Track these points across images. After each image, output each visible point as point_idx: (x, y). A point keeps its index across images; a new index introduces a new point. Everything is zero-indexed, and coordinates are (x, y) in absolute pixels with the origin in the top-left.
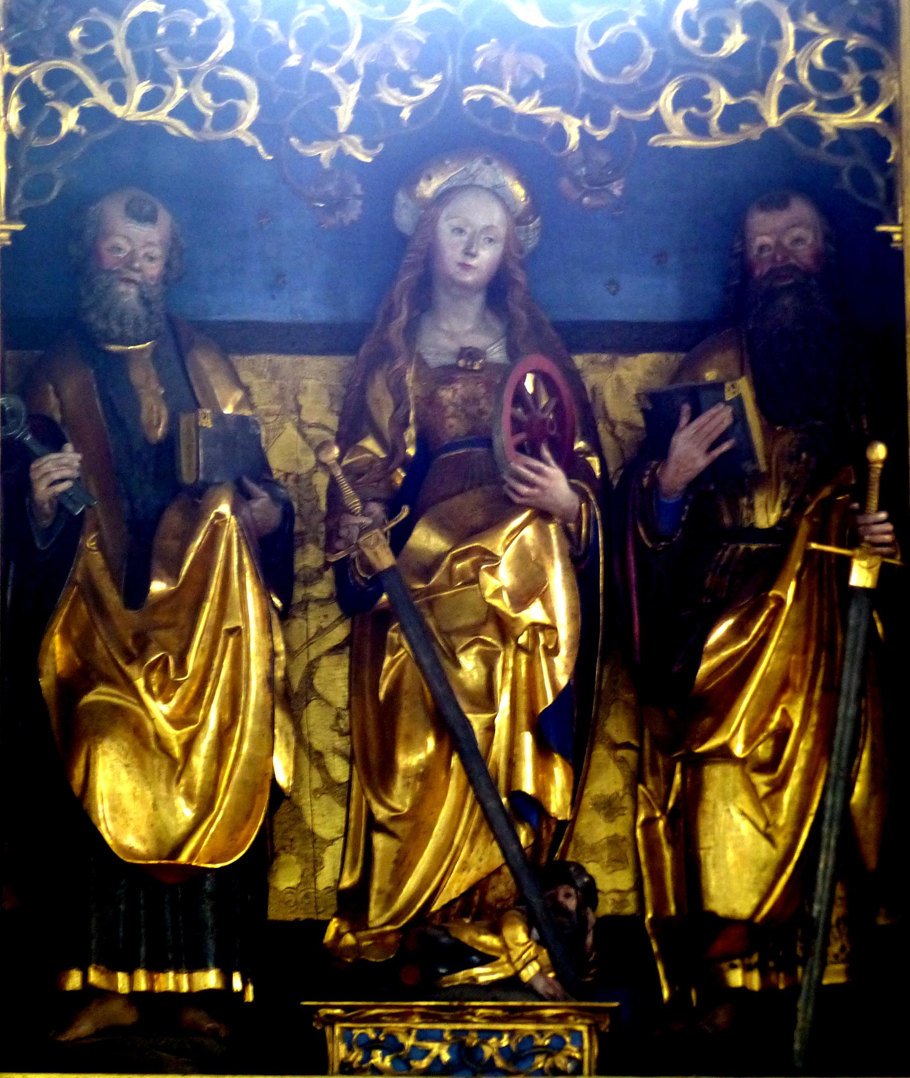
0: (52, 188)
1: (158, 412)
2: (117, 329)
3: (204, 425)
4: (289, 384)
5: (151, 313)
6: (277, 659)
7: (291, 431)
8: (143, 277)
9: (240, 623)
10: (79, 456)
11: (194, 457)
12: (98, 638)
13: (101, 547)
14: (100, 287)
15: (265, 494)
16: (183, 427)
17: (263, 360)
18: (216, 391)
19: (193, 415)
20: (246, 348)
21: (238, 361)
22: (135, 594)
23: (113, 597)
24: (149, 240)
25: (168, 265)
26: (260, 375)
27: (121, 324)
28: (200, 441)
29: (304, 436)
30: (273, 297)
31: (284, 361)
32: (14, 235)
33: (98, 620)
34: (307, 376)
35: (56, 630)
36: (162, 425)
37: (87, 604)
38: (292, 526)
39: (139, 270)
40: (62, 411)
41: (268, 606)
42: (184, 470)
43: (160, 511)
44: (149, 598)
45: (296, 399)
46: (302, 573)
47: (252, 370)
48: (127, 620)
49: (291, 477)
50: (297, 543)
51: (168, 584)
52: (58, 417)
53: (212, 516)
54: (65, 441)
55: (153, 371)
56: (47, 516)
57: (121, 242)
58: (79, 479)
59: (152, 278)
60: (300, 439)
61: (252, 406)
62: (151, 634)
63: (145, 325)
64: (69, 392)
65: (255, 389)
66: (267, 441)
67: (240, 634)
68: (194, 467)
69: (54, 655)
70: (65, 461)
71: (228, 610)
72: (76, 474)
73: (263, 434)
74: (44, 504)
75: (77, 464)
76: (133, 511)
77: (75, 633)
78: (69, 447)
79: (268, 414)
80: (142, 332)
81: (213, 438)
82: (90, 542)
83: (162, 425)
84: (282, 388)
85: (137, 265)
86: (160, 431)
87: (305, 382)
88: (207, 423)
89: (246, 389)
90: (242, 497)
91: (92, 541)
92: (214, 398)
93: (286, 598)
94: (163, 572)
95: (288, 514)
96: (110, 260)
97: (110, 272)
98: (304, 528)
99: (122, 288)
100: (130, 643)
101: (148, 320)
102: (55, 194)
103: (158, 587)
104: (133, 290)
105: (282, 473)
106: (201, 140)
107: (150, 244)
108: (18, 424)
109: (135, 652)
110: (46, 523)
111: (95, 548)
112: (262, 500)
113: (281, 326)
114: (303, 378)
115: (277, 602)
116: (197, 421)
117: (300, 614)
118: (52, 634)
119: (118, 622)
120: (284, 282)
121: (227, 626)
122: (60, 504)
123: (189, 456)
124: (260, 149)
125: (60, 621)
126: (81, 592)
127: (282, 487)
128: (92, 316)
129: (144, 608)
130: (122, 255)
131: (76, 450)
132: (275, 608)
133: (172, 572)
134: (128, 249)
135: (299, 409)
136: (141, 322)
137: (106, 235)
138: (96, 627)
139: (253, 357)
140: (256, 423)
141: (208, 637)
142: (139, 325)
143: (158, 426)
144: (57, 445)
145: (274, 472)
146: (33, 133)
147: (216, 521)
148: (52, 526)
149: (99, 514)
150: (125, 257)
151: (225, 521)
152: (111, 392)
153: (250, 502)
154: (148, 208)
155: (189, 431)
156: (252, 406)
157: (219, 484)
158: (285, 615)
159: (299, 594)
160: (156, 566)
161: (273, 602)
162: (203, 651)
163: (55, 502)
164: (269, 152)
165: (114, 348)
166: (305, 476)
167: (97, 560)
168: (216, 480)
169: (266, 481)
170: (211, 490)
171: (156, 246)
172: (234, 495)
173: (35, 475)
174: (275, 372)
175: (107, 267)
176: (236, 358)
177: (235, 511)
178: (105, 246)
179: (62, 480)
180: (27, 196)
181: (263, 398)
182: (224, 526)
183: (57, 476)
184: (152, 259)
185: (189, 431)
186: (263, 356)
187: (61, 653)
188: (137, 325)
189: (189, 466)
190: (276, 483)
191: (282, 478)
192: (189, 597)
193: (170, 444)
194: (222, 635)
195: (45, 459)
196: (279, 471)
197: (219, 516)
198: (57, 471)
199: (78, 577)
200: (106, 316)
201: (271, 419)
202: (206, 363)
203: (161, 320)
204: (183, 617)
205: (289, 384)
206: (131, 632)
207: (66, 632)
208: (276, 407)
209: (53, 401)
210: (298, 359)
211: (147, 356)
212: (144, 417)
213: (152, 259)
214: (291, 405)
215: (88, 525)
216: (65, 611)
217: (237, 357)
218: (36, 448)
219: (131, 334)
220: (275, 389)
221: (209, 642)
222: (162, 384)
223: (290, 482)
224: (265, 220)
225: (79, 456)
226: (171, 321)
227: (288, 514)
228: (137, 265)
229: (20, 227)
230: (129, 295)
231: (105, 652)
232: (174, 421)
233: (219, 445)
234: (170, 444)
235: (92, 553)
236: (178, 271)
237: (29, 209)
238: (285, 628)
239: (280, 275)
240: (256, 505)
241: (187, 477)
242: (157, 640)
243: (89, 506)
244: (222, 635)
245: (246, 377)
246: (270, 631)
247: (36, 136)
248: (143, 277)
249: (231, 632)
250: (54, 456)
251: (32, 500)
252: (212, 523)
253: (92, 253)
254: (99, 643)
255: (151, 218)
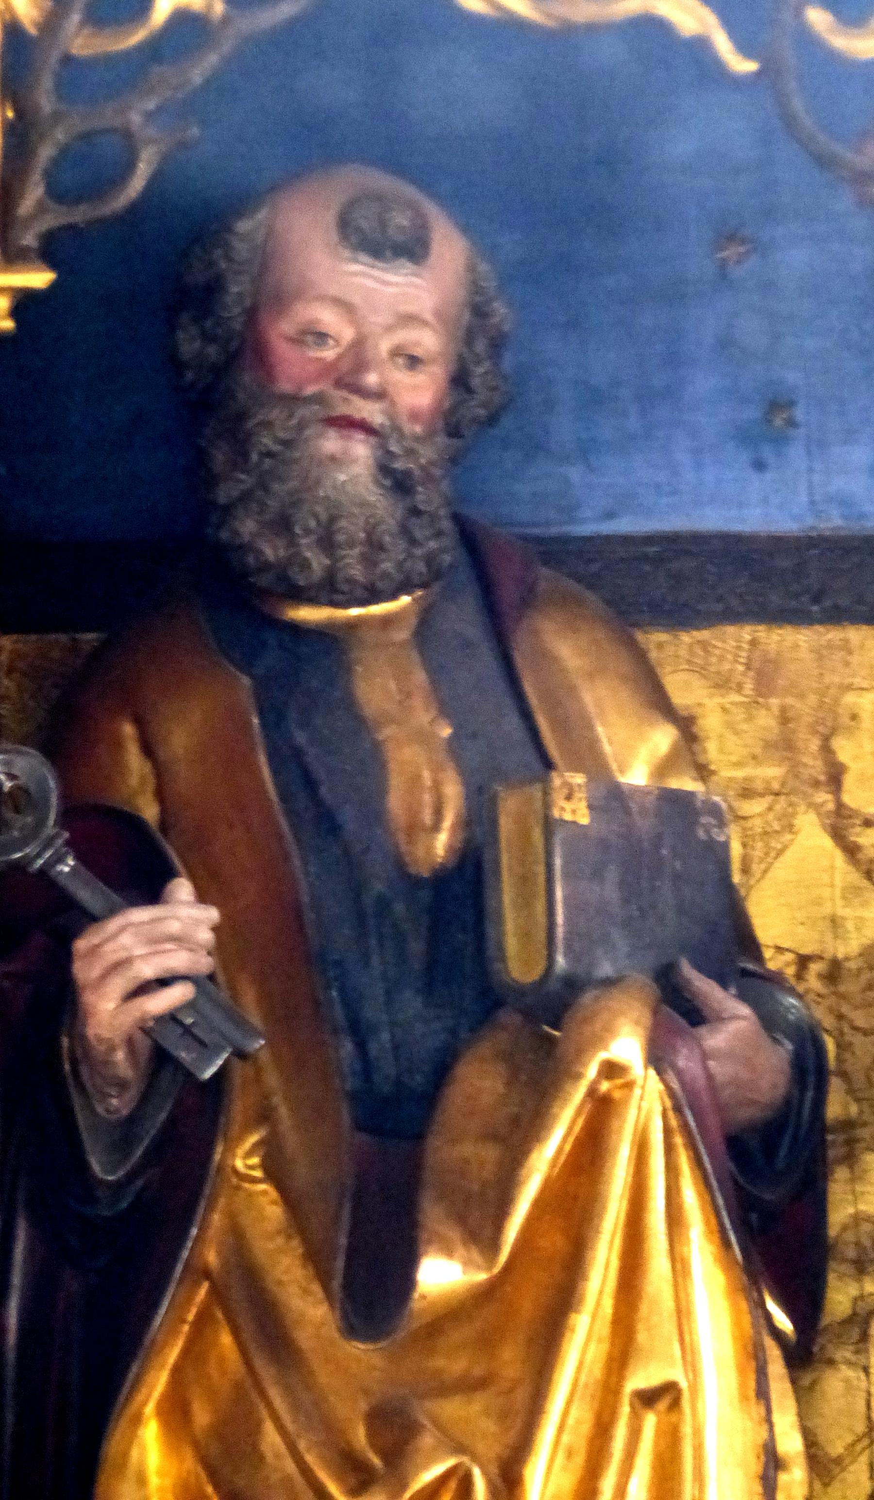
0: (130, 166)
1: (437, 786)
2: (318, 562)
3: (568, 817)
4: (805, 708)
5: (415, 512)
6: (783, 1478)
7: (811, 838)
8: (392, 416)
9: (676, 1374)
10: (212, 914)
11: (540, 907)
12: (269, 1427)
13: (275, 1170)
14: (267, 441)
15: (745, 1010)
16: (506, 825)
17: (734, 640)
18: (600, 730)
19: (536, 791)
20: (681, 615)
21: (660, 646)
22: (373, 1289)
23: (310, 1311)
24: (410, 308)
25: (460, 381)
26: (722, 684)
27: (327, 542)
28: (558, 862)
29: (851, 851)
30: (760, 466)
31: (793, 643)
32: (24, 303)
33: (266, 1372)
34: (857, 681)
35: (150, 1409)
36: (448, 823)
37: (236, 1332)
38: (820, 1102)
39: (380, 395)
40: (160, 795)
41: (754, 1325)
42: (512, 944)
43: (442, 1071)
44: (416, 1303)
45: (827, 750)
46: (850, 1236)
47: (702, 671)
48: (347, 1367)
49: (815, 968)
50: (832, 1153)
51: (467, 1264)
52: (150, 812)
53: (591, 1071)
54: (169, 873)
55: (420, 677)
56: (122, 1085)
57: (328, 318)
58: (211, 977)
59: (414, 416)
60: (839, 858)
61: (703, 772)
62: (426, 1410)
63: (397, 549)
64: (180, 739)
65: (711, 723)
66: (746, 870)
67: (676, 1404)
68: (542, 935)
69: (142, 1480)
70: (174, 927)
71: (642, 1337)
72: (204, 963)
73: (736, 849)
74: (112, 1049)
75: (206, 936)
76: (367, 1067)
77: (202, 1416)
78: (182, 889)
79: (747, 793)
80: (387, 566)
81: (592, 855)
82: (244, 1158)
83: (448, 823)
84: (785, 718)
85: (372, 379)
86: (441, 843)
87: (850, 698)
88: (575, 811)
89: (687, 727)
90: (678, 1012)
91: (249, 1154)
92: (593, 746)
93: (806, 1303)
94: (454, 1234)
95: (809, 1068)
96: (295, 366)
97: (294, 400)
98: (854, 1109)
99: (331, 443)
100: (360, 1436)
101: (405, 531)
102: (137, 184)
103: (441, 1275)
104: (361, 450)
105: (789, 957)
106: (550, 23)
107: (409, 320)
108: (41, 823)
109: (376, 1461)
110: (119, 1104)
111: (258, 1174)
112: (733, 1027)
113: (778, 544)
114: (849, 688)
115: (784, 1322)
116: (547, 805)
117: (844, 1353)
118: (137, 1420)
119: (324, 1376)
120: (792, 423)
121: (640, 1379)
122: (158, 1054)
123: (525, 902)
124: (723, 45)
125: (158, 1382)
126: (217, 1294)
127: (792, 991)
128: (247, 527)
129: (401, 1334)
130: (329, 354)
131: (203, 897)
132: (777, 1334)
133: (482, 1235)
134: (348, 334)
135: (835, 777)
136: (387, 539)
137: (282, 301)
138: (263, 1394)
139: (704, 634)
140: (715, 811)
141: (582, 1416)
142: (381, 548)
143: (436, 828)
144: (146, 885)
145: (768, 954)
146: (76, 18)
147: (605, 1086)
148: (133, 1120)
149: (272, 1079)
150: (340, 357)
151: (629, 1085)
152: (300, 737)
153: (703, 1030)
154: (401, 219)
155: (525, 836)
156: (703, 772)
157: (609, 983)
158: (802, 1356)
159: (841, 1296)
160: (433, 1214)
161: (768, 1317)
162: (570, 1454)
163: (144, 1044)
164: (745, 48)
165: (308, 614)
166: (852, 965)
167: (266, 1206)
168: (605, 969)
169: (745, 973)
170: (587, 998)
171: (425, 323)
172: (655, 1012)
173: (84, 971)
174: (766, 676)
175: (285, 386)
176: (656, 641)
177: (657, 1057)
178: (280, 331)
179: (163, 982)
180: (57, 193)
181: (734, 743)
182: (626, 1101)
183: (148, 970)
184: (414, 362)
185: (525, 836)
186: (730, 630)
187: (161, 1474)
188: (374, 546)
189: (525, 935)
190: (775, 979)
191: (790, 971)
192: (528, 1303)
193: (467, 882)
194: (625, 1409)
195: (113, 925)
196: (779, 949)
197: (611, 1070)
198: (147, 958)
199: (212, 1257)
200: (283, 525)
201: (753, 807)
202: (567, 650)
203: (439, 534)
204: (511, 1359)
205: (805, 708)
206: (363, 1406)
207: (176, 1412)
208: (772, 772)
209: (135, 761)
210: (833, 635)
211: (402, 635)
212: (395, 803)
213: (414, 362)
214: (815, 766)
215: (239, 1106)
216: (173, 1354)
217: (662, 637)
218: (87, 894)
219: (357, 572)
220: (766, 721)
221: (586, 1428)
222: (446, 709)
223: (813, 981)
224: (731, 252)
225: (212, 914)
226: (469, 538)
227: (809, 1068)
228: (372, 379)
229: (39, 279)
230: (350, 466)
231: (291, 1467)
232: (479, 820)
233: (612, 874)
234: (467, 882)
235: (249, 1191)
236: (487, 397)
237: (71, 228)
238: (805, 1396)
239: (778, 404)
240: (717, 1039)
241: (519, 962)
242: (437, 1424)
243: (240, 1054)
244: (625, 1409)
245: (684, 690)
246: (763, 1393)
247: (83, 23)
248: (392, 416)
249: (647, 1398)
250: (140, 915)
251: (80, 1038)
252: (592, 1092)
253: (245, 349)
254: (271, 1439)
255: (412, 249)
